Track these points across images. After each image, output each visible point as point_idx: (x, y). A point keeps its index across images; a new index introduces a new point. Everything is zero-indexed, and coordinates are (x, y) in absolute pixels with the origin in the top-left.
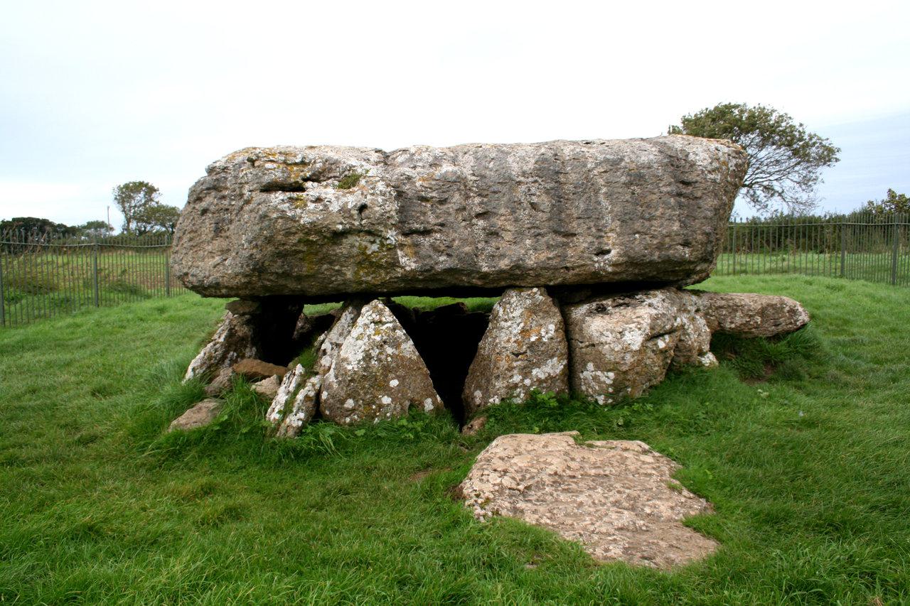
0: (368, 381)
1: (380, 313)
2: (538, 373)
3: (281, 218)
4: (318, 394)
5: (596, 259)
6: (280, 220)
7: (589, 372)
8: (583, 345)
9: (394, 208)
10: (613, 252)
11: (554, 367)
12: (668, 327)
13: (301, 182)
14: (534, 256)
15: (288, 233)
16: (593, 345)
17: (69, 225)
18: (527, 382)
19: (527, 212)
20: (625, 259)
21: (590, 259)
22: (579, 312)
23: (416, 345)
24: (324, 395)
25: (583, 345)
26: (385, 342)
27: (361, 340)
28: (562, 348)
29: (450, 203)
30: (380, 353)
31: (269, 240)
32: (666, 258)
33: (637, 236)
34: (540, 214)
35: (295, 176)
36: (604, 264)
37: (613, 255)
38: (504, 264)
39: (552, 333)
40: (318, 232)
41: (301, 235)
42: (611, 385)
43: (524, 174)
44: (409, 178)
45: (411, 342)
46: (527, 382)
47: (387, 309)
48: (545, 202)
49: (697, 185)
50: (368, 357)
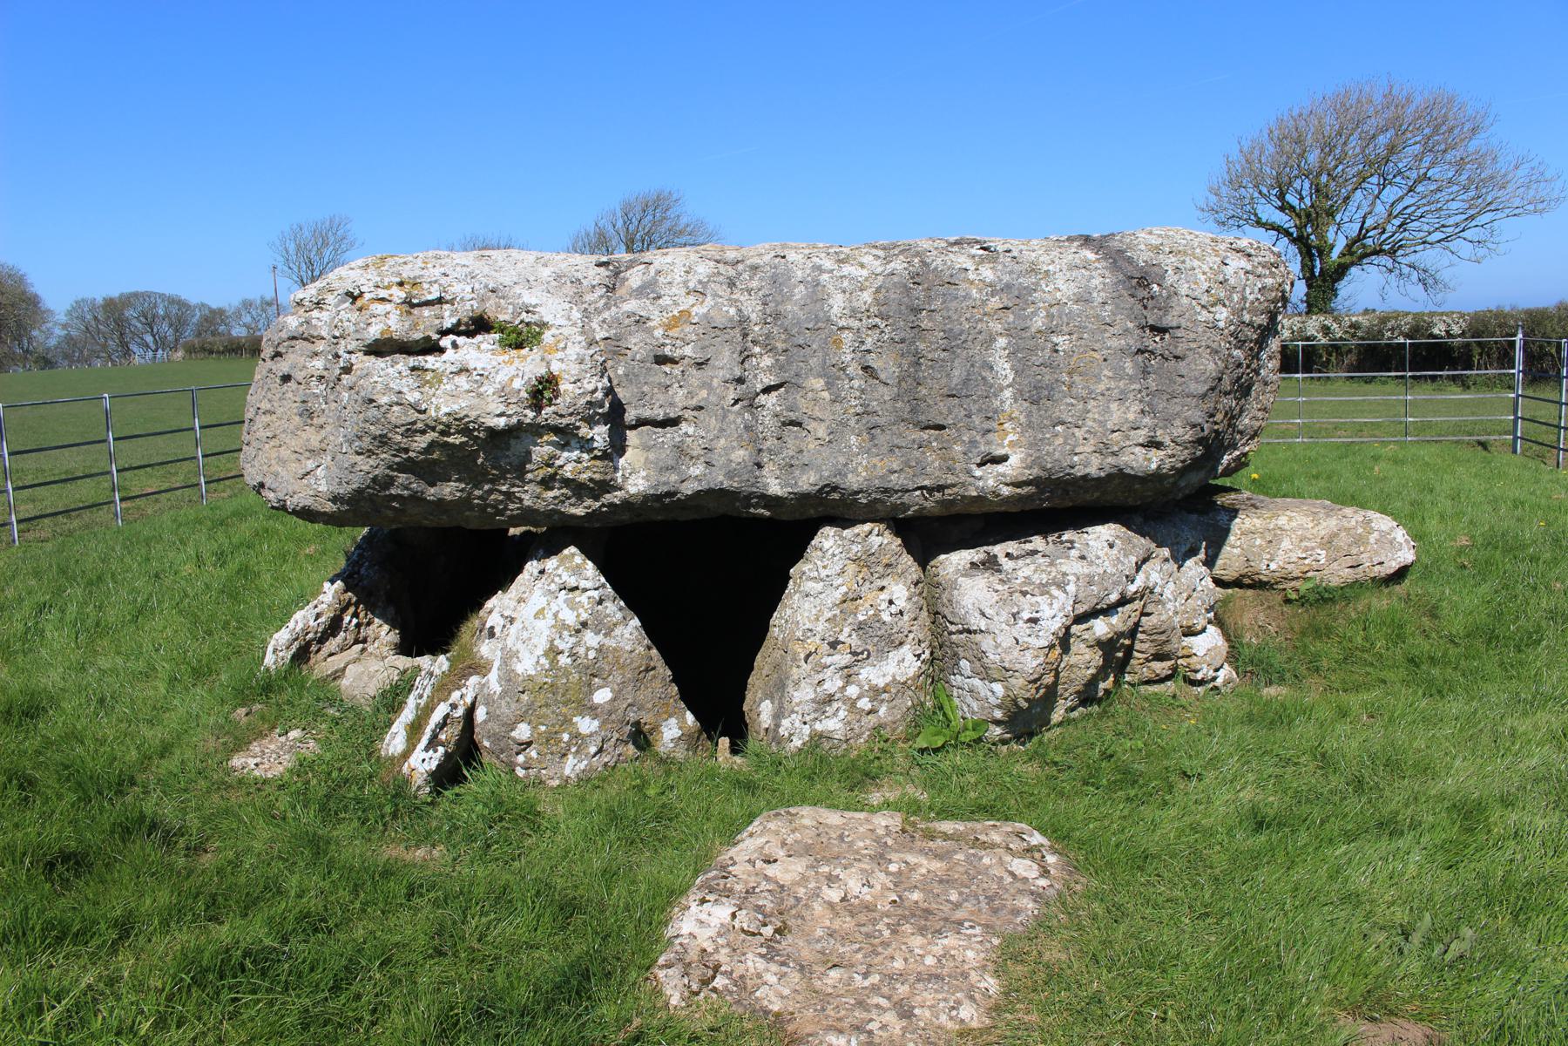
0: (561, 691)
1: (577, 571)
2: (876, 674)
4: (470, 711)
5: (978, 473)
6: (395, 408)
7: (965, 678)
8: (953, 628)
9: (600, 385)
10: (1014, 460)
11: (903, 664)
12: (1114, 597)
13: (435, 337)
14: (861, 468)
15: (411, 431)
16: (969, 632)
17: (214, 306)
18: (852, 691)
19: (856, 383)
20: (1036, 471)
21: (969, 472)
22: (954, 562)
23: (649, 627)
24: (480, 714)
25: (953, 628)
26: (584, 624)
27: (549, 615)
28: (921, 631)
29: (714, 367)
30: (578, 644)
31: (383, 441)
32: (1114, 471)
33: (1059, 428)
34: (882, 389)
35: (426, 323)
36: (993, 481)
37: (1014, 466)
38: (807, 482)
39: (901, 603)
40: (465, 431)
41: (431, 436)
42: (999, 707)
43: (854, 314)
44: (641, 321)
45: (636, 622)
46: (852, 691)
47: (590, 564)
48: (887, 366)
50: (553, 652)
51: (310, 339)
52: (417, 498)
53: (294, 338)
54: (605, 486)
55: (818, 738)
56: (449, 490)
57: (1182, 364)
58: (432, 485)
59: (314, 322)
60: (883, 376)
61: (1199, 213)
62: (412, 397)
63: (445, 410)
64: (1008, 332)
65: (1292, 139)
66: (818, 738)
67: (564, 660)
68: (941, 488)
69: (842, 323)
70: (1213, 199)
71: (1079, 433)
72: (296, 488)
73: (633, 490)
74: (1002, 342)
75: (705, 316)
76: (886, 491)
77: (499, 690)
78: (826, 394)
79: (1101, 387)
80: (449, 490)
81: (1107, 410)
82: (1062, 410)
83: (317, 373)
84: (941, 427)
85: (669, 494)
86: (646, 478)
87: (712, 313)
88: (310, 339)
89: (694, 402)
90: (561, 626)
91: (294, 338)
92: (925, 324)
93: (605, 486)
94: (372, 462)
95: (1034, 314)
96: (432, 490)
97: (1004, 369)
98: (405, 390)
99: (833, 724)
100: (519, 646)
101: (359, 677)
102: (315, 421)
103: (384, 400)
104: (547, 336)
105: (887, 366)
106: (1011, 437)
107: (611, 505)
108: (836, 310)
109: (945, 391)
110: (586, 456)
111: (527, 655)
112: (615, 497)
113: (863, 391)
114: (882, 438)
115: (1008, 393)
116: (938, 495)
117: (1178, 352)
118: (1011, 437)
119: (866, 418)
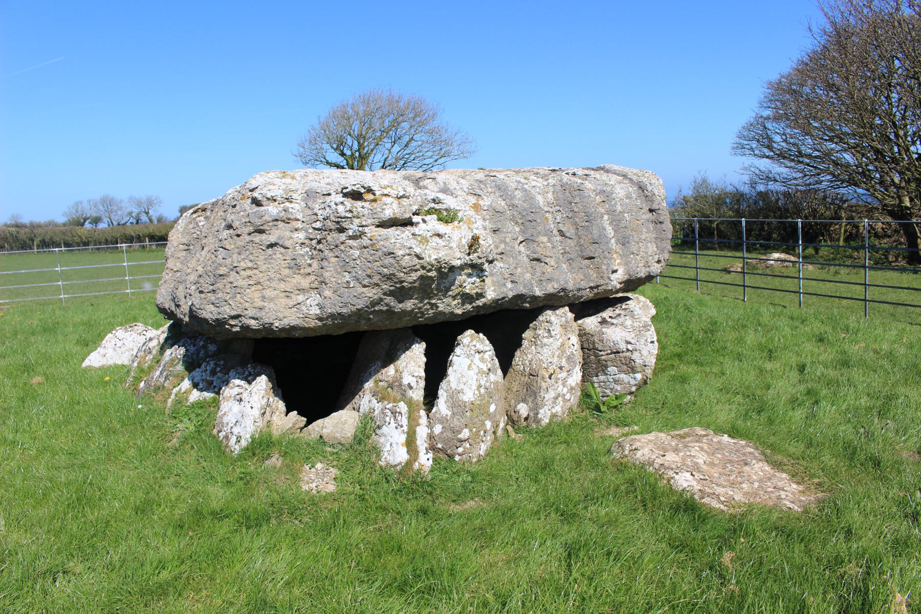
3: (409, 255)
6: (407, 257)
10: (620, 271)
25: (602, 353)
49: (660, 212)
51: (287, 221)
52: (390, 312)
53: (277, 220)
54: (480, 295)
55: (554, 416)
56: (409, 305)
57: (663, 225)
58: (400, 302)
59: (290, 210)
60: (568, 235)
61: (296, 159)
62: (418, 250)
63: (434, 257)
64: (608, 213)
65: (343, 117)
66: (554, 416)
67: (482, 391)
68: (597, 287)
69: (546, 209)
70: (302, 150)
71: (638, 258)
72: (287, 314)
73: (489, 298)
74: (606, 217)
75: (490, 206)
76: (579, 290)
77: (449, 413)
78: (549, 244)
79: (643, 237)
80: (409, 305)
81: (647, 247)
82: (634, 249)
83: (301, 241)
84: (593, 258)
85: (503, 298)
86: (494, 291)
87: (494, 204)
88: (287, 221)
89: (499, 251)
90: (481, 372)
91: (277, 220)
92: (576, 209)
93: (480, 295)
94: (374, 291)
95: (616, 204)
96: (400, 306)
97: (610, 231)
98: (414, 246)
99: (558, 409)
100: (462, 386)
101: (335, 426)
102: (302, 271)
103: (401, 253)
104: (460, 214)
105: (569, 230)
106: (618, 261)
107: (478, 307)
108: (541, 203)
109: (592, 241)
110: (478, 280)
111: (468, 390)
112: (479, 303)
113: (561, 242)
114: (574, 265)
115: (613, 241)
116: (596, 290)
117: (661, 220)
118: (618, 261)
119: (566, 256)
